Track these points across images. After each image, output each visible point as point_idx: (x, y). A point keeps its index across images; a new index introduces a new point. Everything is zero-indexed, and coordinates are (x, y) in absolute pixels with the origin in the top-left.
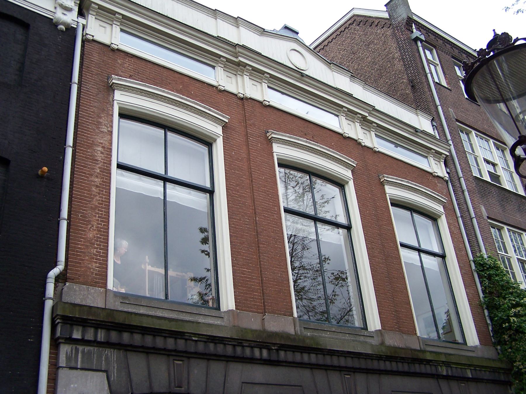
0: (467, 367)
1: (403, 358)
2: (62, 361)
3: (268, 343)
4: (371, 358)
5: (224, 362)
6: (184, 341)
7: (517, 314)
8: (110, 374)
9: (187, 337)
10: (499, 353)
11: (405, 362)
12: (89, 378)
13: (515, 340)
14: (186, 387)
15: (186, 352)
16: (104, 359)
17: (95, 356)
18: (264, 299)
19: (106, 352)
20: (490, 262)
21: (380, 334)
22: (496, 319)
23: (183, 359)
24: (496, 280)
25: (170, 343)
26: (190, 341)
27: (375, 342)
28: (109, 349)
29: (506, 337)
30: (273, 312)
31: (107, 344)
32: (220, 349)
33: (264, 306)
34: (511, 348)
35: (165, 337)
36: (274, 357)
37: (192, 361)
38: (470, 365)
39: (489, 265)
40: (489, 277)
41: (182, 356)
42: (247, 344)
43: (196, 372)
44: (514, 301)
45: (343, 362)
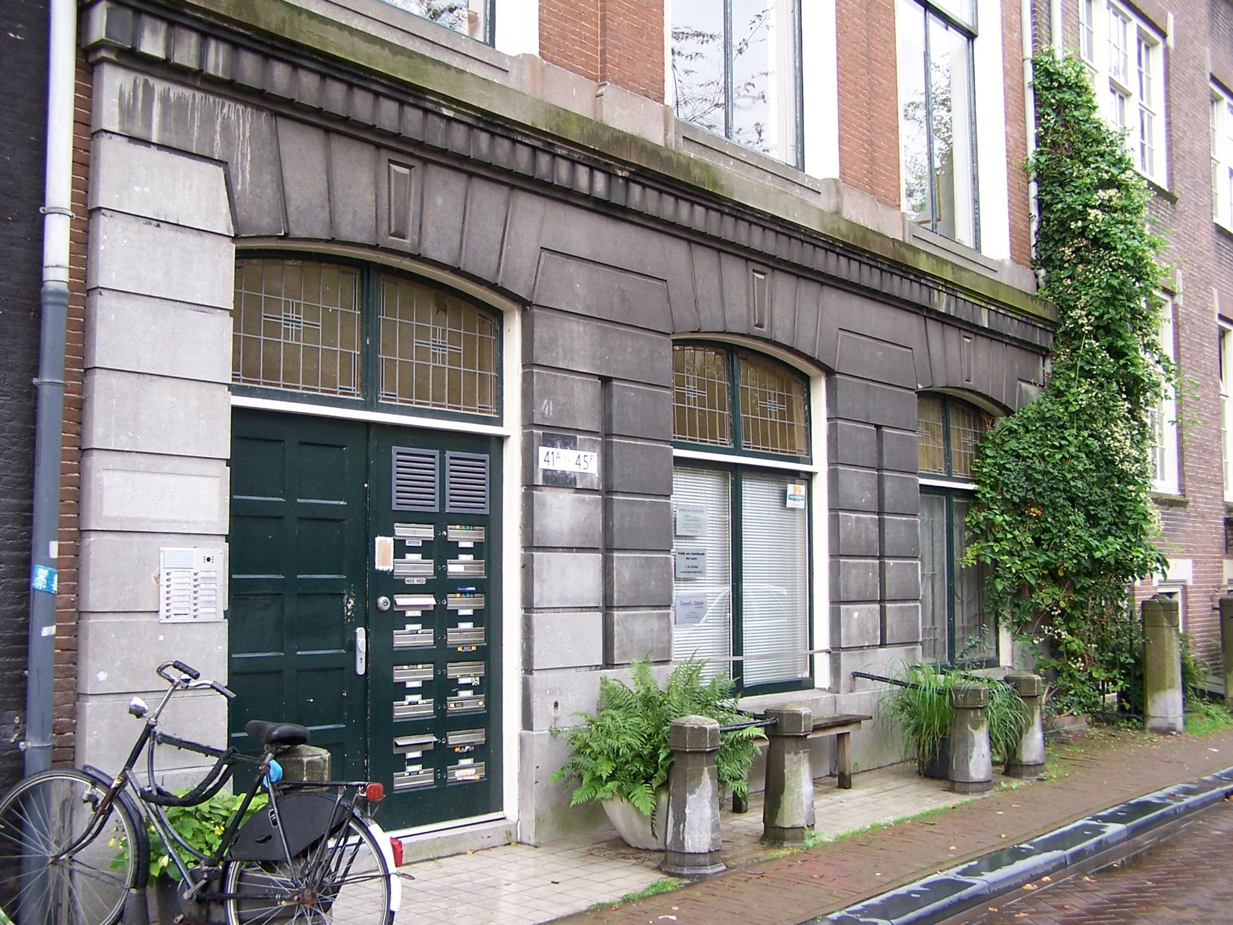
0: (983, 304)
1: (874, 256)
2: (109, 115)
3: (611, 158)
4: (814, 242)
5: (505, 189)
6: (420, 113)
7: (1105, 203)
8: (233, 171)
9: (429, 106)
10: (1038, 287)
11: (877, 268)
12: (182, 174)
13: (1083, 261)
14: (416, 238)
15: (420, 145)
16: (218, 128)
17: (197, 115)
18: (603, 42)
19: (225, 111)
20: (1070, 73)
21: (834, 190)
22: (1059, 206)
23: (411, 162)
24: (1073, 116)
25: (388, 114)
26: (436, 119)
27: (825, 203)
28: (232, 104)
29: (1068, 251)
30: (621, 82)
31: (230, 88)
32: (501, 153)
33: (604, 62)
34: (1071, 277)
35: (377, 94)
36: (618, 199)
37: (433, 171)
38: (990, 300)
39: (1066, 79)
40: (1060, 108)
41: (411, 155)
42: (564, 152)
43: (440, 201)
44: (1107, 172)
45: (757, 239)
